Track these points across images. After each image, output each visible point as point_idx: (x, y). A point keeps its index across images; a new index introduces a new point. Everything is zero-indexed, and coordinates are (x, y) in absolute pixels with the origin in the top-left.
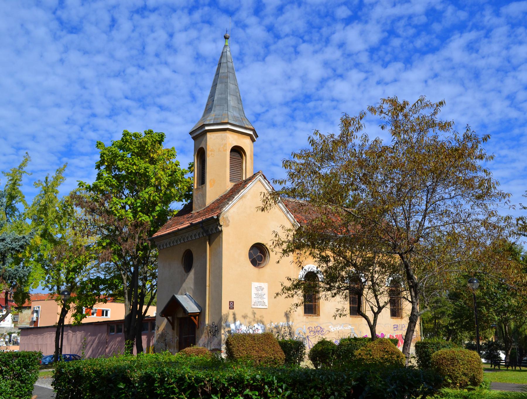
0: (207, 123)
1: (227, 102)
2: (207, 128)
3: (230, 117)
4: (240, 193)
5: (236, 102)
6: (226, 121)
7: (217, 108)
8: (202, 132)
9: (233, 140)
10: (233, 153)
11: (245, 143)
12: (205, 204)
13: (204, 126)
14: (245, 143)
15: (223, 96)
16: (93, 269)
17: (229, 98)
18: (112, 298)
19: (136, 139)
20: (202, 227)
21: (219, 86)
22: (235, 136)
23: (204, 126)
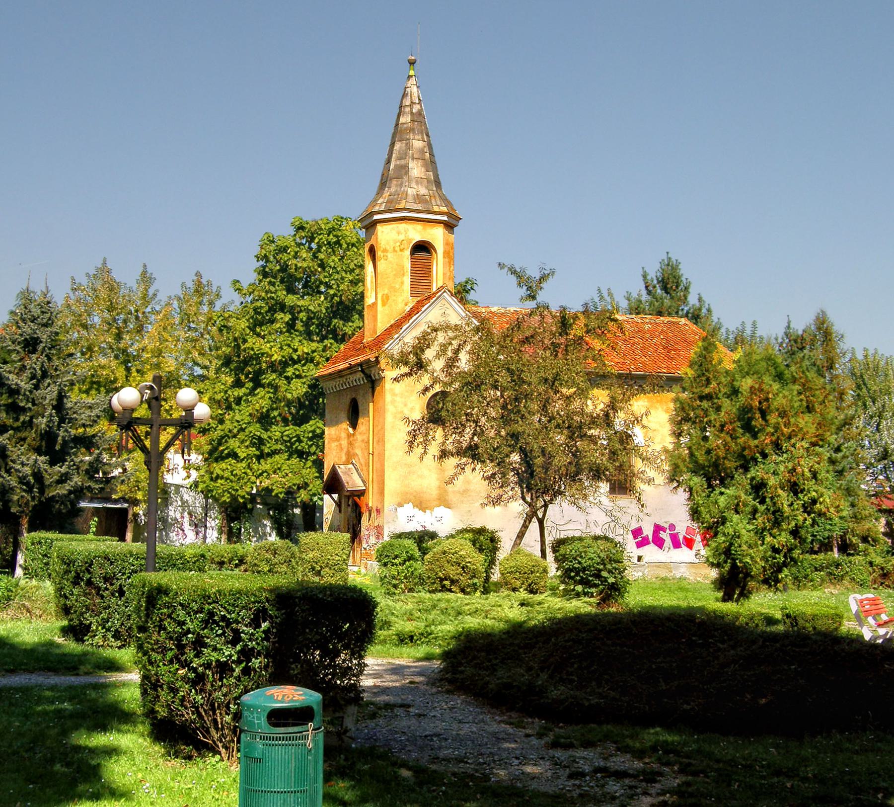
0: (376, 209)
1: (407, 173)
2: (376, 217)
3: (410, 199)
4: (411, 321)
5: (423, 169)
6: (401, 206)
7: (394, 182)
8: (370, 223)
9: (416, 233)
10: (416, 255)
11: (436, 236)
12: (376, 333)
13: (372, 214)
14: (436, 236)
15: (403, 162)
16: (724, 333)
17: (411, 165)
18: (136, 415)
19: (112, 584)
20: (363, 371)
21: (398, 146)
22: (419, 226)
23: (372, 214)
